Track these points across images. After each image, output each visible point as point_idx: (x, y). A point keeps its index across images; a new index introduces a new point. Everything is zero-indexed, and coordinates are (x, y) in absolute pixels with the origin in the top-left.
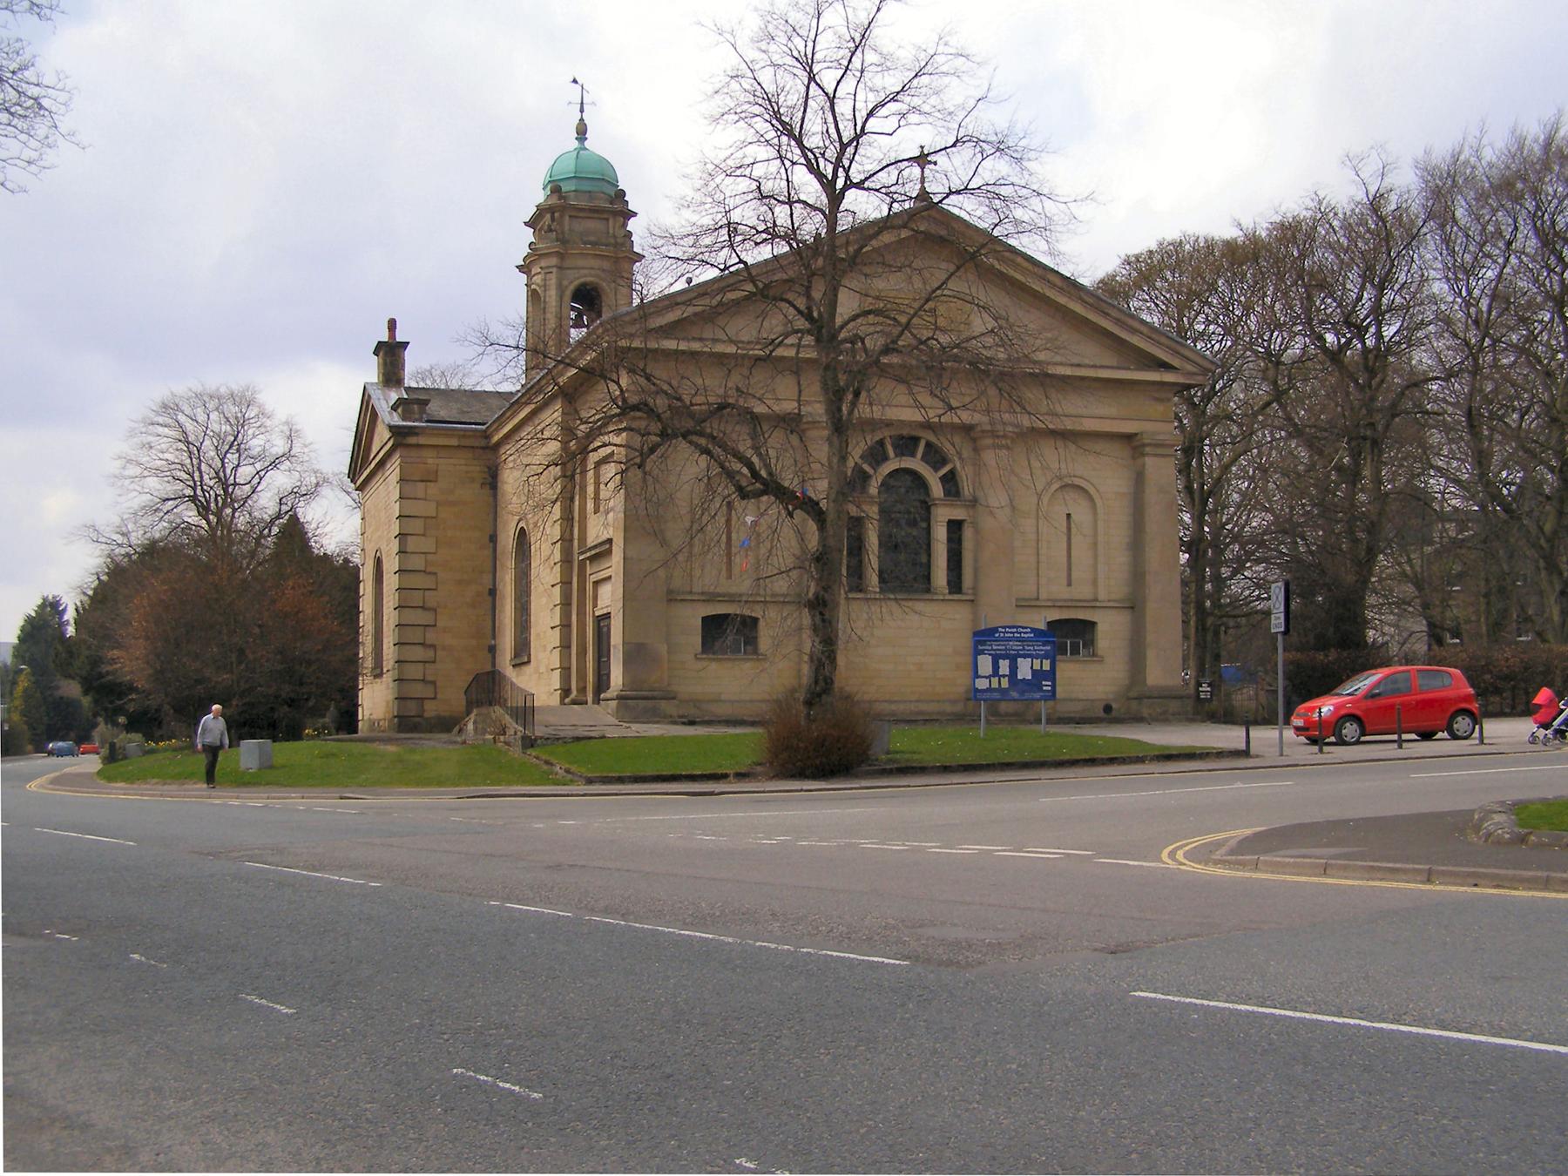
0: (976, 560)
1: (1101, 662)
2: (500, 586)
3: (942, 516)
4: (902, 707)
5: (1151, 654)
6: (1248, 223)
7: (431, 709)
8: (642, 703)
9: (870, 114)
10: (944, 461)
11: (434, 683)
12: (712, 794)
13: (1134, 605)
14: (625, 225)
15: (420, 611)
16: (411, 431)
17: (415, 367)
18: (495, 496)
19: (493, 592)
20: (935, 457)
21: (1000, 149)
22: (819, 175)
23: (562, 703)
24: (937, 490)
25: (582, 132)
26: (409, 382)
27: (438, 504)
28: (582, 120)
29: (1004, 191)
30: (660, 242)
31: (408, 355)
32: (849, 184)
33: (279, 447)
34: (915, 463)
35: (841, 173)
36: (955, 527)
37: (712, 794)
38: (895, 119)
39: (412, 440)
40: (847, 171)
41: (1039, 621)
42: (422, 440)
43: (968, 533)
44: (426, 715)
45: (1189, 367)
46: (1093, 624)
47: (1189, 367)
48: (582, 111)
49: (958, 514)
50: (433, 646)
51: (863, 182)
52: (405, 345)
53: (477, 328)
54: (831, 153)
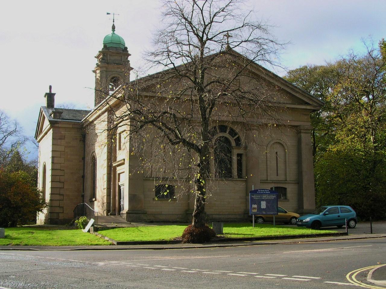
0: (247, 167)
1: (288, 201)
2: (86, 175)
3: (236, 152)
4: (223, 216)
5: (305, 199)
6: (328, 61)
7: (61, 216)
8: (135, 215)
9: (215, 16)
10: (236, 134)
11: (63, 207)
12: (163, 249)
13: (299, 182)
14: (127, 58)
15: (58, 183)
16: (56, 122)
17: (58, 103)
18: (84, 145)
19: (83, 177)
20: (233, 133)
21: (259, 27)
22: (197, 35)
23: (107, 215)
24: (233, 144)
25: (114, 28)
26: (56, 106)
27: (65, 147)
28: (114, 25)
29: (260, 41)
30: (144, 56)
31: (56, 97)
32: (208, 39)
33: (12, 128)
34: (226, 135)
35: (205, 35)
36: (239, 155)
37: (163, 249)
38: (222, 17)
39: (57, 125)
40: (207, 35)
41: (268, 187)
42: (60, 125)
43: (244, 158)
44: (60, 218)
45: (316, 105)
46: (285, 189)
47: (316, 105)
48: (114, 22)
49: (241, 151)
50: (63, 195)
51: (212, 38)
52: (54, 94)
53: (79, 93)
54: (202, 29)
